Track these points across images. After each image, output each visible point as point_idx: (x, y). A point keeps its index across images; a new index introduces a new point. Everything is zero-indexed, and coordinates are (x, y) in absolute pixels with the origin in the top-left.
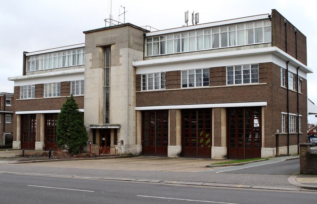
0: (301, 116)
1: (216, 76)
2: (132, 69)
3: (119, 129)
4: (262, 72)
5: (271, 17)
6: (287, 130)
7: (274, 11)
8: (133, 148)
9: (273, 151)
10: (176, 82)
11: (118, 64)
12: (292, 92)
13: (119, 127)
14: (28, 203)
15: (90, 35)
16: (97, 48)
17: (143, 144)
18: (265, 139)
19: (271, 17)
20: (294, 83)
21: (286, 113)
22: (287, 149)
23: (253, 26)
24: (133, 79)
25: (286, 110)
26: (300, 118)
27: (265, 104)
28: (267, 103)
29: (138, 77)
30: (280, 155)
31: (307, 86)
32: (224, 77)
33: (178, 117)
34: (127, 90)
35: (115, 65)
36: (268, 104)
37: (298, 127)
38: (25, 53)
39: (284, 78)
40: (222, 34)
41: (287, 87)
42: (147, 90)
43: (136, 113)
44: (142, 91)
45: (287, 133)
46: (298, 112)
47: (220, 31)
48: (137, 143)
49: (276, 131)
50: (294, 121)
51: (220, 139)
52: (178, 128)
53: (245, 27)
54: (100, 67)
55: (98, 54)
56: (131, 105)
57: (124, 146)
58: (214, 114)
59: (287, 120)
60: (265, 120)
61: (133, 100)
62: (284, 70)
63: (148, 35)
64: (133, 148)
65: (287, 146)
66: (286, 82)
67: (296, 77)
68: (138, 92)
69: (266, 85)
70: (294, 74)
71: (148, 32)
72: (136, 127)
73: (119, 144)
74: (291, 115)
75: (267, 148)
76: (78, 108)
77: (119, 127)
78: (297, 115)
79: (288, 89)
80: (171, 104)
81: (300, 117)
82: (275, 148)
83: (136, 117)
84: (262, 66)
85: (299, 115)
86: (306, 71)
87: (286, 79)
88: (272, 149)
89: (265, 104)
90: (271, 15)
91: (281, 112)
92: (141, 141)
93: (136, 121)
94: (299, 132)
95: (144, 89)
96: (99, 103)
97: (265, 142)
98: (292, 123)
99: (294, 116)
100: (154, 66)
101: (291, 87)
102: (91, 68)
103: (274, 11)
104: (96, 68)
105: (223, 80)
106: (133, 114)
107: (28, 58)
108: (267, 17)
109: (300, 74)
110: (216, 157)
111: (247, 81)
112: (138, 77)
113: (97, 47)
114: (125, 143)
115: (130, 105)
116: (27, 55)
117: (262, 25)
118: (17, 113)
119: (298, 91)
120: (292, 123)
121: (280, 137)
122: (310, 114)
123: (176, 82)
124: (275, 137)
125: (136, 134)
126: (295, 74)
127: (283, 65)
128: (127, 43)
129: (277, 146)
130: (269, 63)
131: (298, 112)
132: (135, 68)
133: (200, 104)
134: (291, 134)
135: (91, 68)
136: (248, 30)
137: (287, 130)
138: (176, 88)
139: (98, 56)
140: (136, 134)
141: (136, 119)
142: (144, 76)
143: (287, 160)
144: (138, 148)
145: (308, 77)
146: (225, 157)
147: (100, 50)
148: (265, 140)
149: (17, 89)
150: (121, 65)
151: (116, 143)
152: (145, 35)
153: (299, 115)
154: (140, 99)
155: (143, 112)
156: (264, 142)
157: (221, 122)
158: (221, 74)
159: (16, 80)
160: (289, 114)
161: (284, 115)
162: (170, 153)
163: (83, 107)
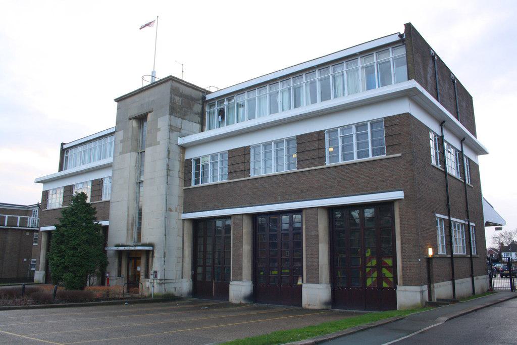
0: (474, 225)
1: (307, 149)
2: (178, 150)
3: (153, 251)
4: (391, 134)
5: (405, 37)
6: (450, 244)
7: (409, 27)
8: (174, 285)
9: (422, 292)
10: (242, 167)
11: (155, 143)
12: (455, 180)
13: (151, 248)
14: (144, 344)
15: (122, 102)
16: (131, 121)
17: (194, 277)
18: (403, 267)
19: (405, 37)
20: (457, 166)
21: (447, 218)
22: (451, 287)
23: (374, 59)
24: (177, 167)
25: (447, 213)
26: (472, 229)
27: (399, 195)
28: (405, 193)
29: (187, 164)
30: (438, 300)
31: (479, 176)
32: (323, 150)
33: (246, 228)
34: (165, 185)
35: (150, 145)
36: (405, 196)
37: (470, 246)
38: (62, 144)
39: (438, 151)
40: (321, 80)
41: (445, 168)
42: (201, 185)
43: (183, 224)
44: (193, 185)
45: (449, 256)
46: (468, 218)
47: (317, 75)
48: (184, 276)
49: (426, 252)
50: (462, 233)
51: (317, 268)
52: (247, 248)
53: (360, 62)
54: (132, 151)
55: (130, 130)
56: (173, 208)
57: (158, 281)
58: (306, 220)
59: (448, 230)
60: (401, 228)
61: (176, 200)
62: (437, 137)
63: (208, 97)
64: (174, 285)
65: (451, 280)
66: (442, 159)
67: (460, 156)
68: (187, 188)
69: (400, 157)
70: (456, 150)
71: (209, 92)
72: (183, 248)
73: (152, 277)
74: (455, 222)
75: (408, 288)
76: (95, 219)
77: (151, 248)
78: (467, 223)
79: (445, 172)
80: (245, 206)
81: (473, 226)
82: (425, 287)
83: (183, 230)
84: (390, 122)
85: (471, 224)
86: (479, 150)
87: (441, 154)
88: (418, 288)
89: (399, 195)
90: (403, 34)
91: (434, 212)
92: (192, 272)
93: (183, 237)
94: (473, 254)
95: (197, 182)
96: (128, 209)
97: (403, 275)
98: (458, 237)
99: (462, 224)
100: (210, 146)
101: (452, 169)
102: (121, 154)
103: (409, 27)
104: (127, 153)
105: (321, 156)
106: (175, 225)
107: (67, 151)
108: (397, 38)
109: (467, 153)
110: (309, 305)
111: (314, 101)
112: (187, 164)
113: (130, 119)
114: (159, 277)
115: (170, 210)
116: (65, 147)
117: (390, 55)
118: (42, 229)
119: (465, 180)
120: (458, 237)
121: (434, 263)
122: (488, 224)
123: (242, 167)
124: (425, 264)
125: (183, 260)
126: (459, 151)
127: (434, 127)
128: (256, 152)
129: (430, 282)
130: (403, 114)
131: (468, 218)
132: (184, 148)
133: (281, 203)
134: (458, 257)
135: (121, 154)
136: (366, 67)
137: (450, 244)
138: (242, 177)
139: (130, 134)
140: (183, 260)
141: (183, 234)
142: (198, 161)
143: (450, 319)
144: (185, 286)
145: (481, 160)
146: (326, 303)
147: (134, 124)
148: (403, 270)
149: (45, 194)
150: (159, 143)
151: (147, 276)
152: (204, 98)
153: (471, 224)
154: (191, 199)
155: (195, 222)
156: (401, 273)
157: (317, 236)
158: (316, 145)
159: (44, 182)
160: (452, 219)
161: (441, 219)
162: (232, 295)
163: (106, 218)
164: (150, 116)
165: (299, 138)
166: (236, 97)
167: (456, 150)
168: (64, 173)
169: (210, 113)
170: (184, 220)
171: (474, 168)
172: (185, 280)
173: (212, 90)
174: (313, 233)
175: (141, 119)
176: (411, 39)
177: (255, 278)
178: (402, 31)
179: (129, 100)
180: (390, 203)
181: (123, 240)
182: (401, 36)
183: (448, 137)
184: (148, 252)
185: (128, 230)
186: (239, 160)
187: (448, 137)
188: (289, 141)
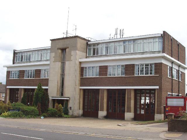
5: (163, 35)
10: (104, 73)
13: (68, 99)
15: (54, 41)
19: (163, 35)
43: (80, 90)
54: (59, 61)
61: (78, 82)
70: (177, 70)
71: (89, 41)
100: (93, 64)
106: (78, 91)
109: (181, 70)
118: (8, 87)
123: (104, 73)
127: (170, 64)
132: (80, 63)
144: (81, 112)
147: (60, 51)
154: (84, 81)
164: (67, 50)
165: (126, 65)
166: (100, 45)
167: (177, 70)
168: (15, 65)
169: (89, 49)
170: (80, 89)
171: (183, 74)
172: (80, 110)
173: (92, 40)
174: (130, 97)
175: (63, 50)
176: (165, 36)
177: (108, 110)
178: (162, 33)
179: (57, 41)
180: (154, 90)
181: (55, 95)
182: (162, 35)
183: (174, 66)
184: (67, 100)
185: (57, 91)
186: (103, 69)
187: (174, 66)
188: (122, 66)
